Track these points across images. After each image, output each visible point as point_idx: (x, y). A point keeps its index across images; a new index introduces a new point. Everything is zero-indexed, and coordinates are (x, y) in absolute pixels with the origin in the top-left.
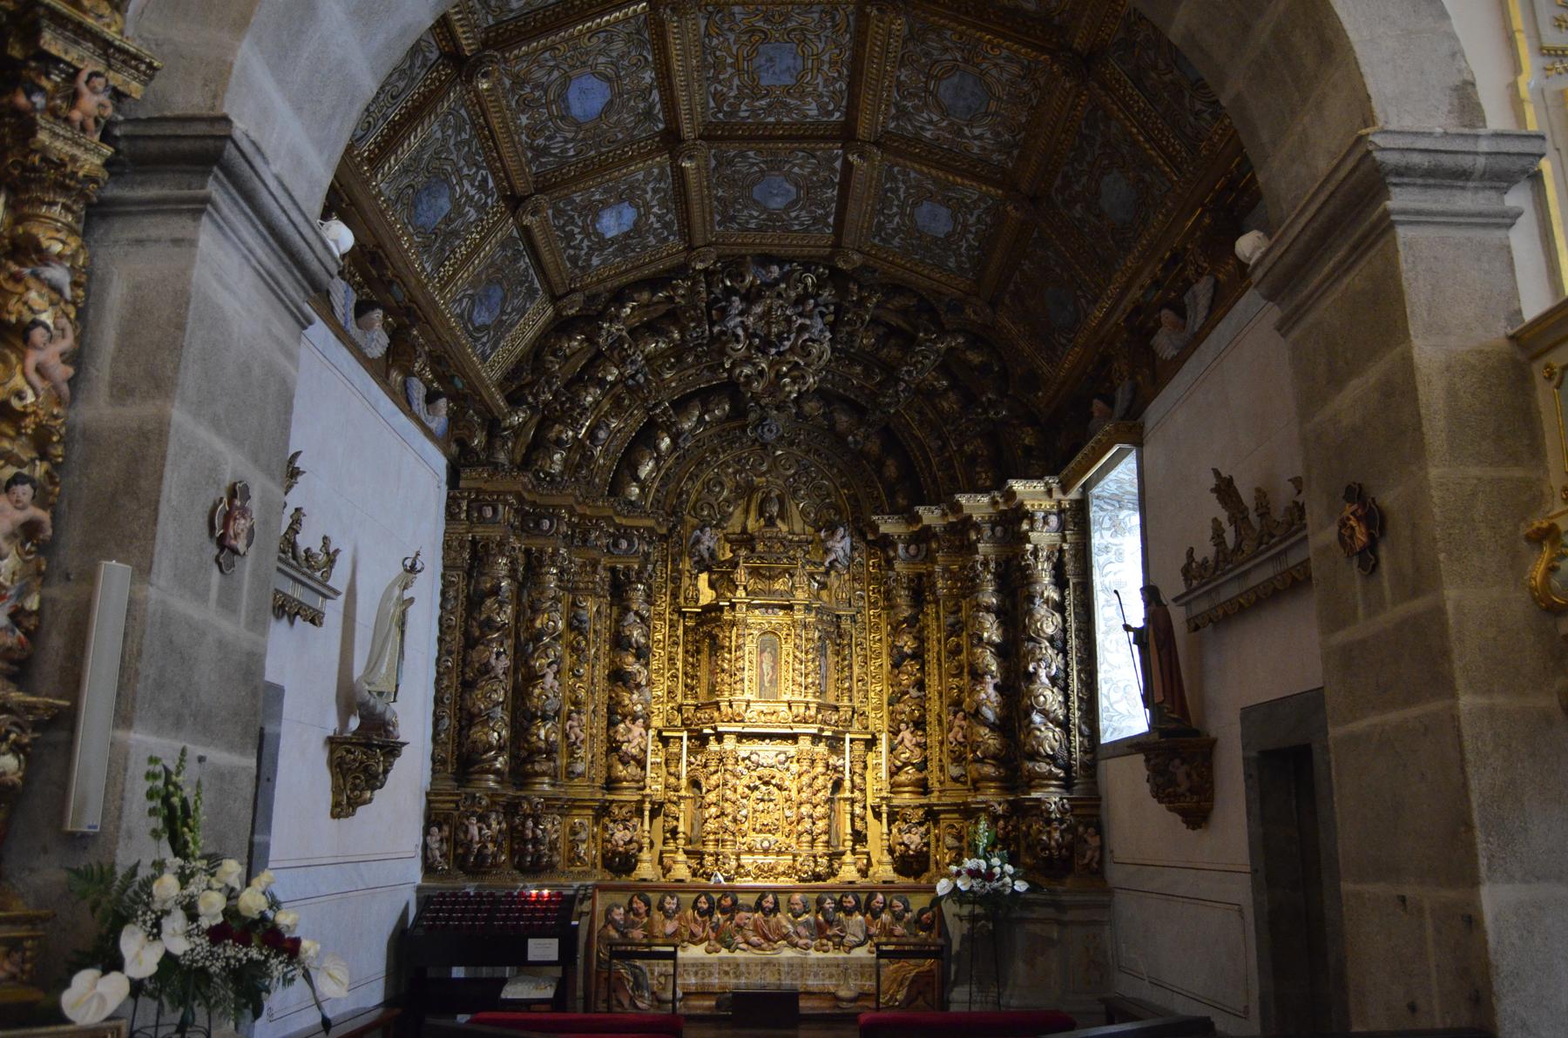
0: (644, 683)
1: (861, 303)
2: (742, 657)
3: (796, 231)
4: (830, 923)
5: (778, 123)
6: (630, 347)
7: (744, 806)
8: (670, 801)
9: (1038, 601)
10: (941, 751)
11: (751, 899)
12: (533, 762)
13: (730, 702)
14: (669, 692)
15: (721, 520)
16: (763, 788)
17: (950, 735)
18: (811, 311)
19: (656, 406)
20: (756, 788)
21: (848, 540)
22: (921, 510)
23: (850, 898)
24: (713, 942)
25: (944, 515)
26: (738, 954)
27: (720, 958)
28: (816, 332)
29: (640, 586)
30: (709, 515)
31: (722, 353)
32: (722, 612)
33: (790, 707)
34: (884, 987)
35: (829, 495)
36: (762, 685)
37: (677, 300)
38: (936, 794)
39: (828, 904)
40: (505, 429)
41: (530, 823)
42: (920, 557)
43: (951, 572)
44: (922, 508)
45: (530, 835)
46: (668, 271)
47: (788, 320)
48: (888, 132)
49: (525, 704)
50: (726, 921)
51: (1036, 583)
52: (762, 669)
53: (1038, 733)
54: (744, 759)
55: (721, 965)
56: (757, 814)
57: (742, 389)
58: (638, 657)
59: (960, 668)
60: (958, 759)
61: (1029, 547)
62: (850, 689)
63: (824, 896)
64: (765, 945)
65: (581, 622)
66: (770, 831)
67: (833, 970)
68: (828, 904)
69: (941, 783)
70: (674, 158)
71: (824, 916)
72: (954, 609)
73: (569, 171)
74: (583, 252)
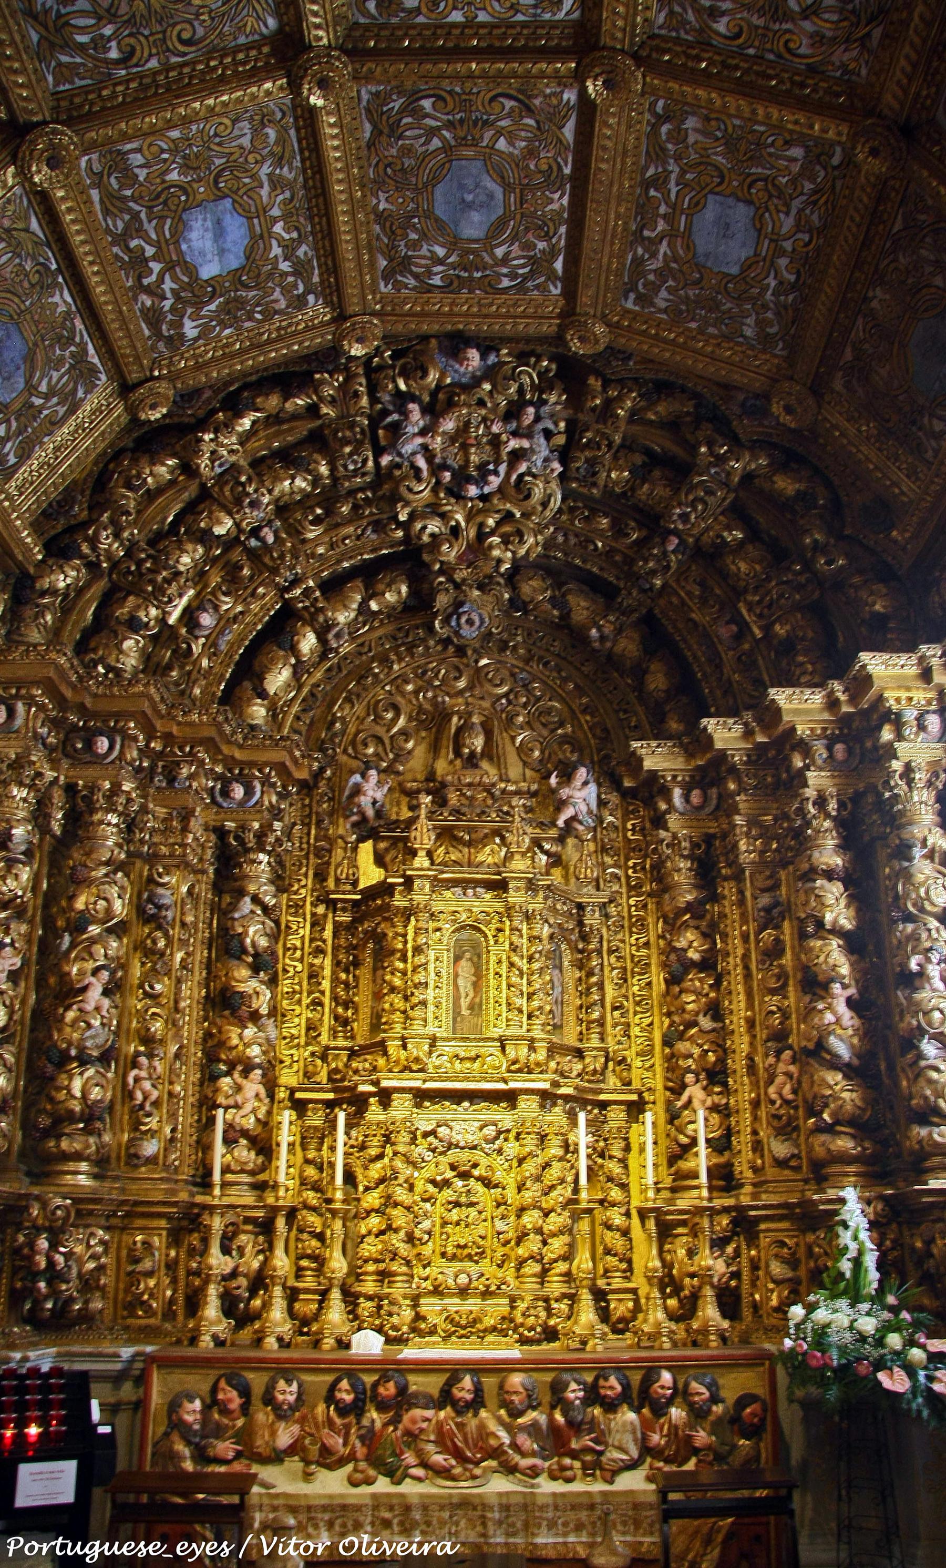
0: (264, 1011)
1: (606, 412)
2: (425, 966)
3: (505, 290)
4: (575, 1427)
5: (470, 23)
6: (250, 480)
7: (426, 1215)
8: (306, 1206)
9: (917, 852)
10: (755, 1118)
11: (432, 1384)
12: (58, 1137)
13: (403, 1038)
14: (308, 1029)
15: (395, 760)
16: (459, 1183)
17: (772, 1090)
18: (530, 426)
19: (295, 582)
20: (447, 1183)
21: (592, 788)
22: (710, 724)
23: (613, 1381)
24: (362, 1465)
25: (748, 734)
26: (408, 1488)
27: (374, 1496)
28: (538, 459)
29: (263, 857)
30: (376, 754)
31: (395, 498)
32: (392, 895)
33: (503, 1048)
34: (676, 1549)
35: (561, 724)
36: (457, 1013)
37: (325, 410)
38: (748, 1189)
39: (574, 1393)
40: (43, 594)
41: (43, 1243)
42: (708, 810)
43: (760, 825)
44: (713, 721)
45: (43, 1264)
46: (306, 358)
47: (496, 442)
48: (652, 37)
49: (51, 1036)
50: (386, 1425)
51: (911, 823)
52: (456, 986)
53: (934, 1075)
54: (426, 1135)
55: (376, 1508)
56: (449, 1229)
57: (426, 557)
58: (256, 969)
59: (782, 976)
60: (786, 1129)
61: (897, 765)
62: (601, 1022)
63: (566, 1376)
64: (458, 1471)
65: (159, 907)
66: (470, 1257)
67: (583, 1515)
68: (574, 1393)
69: (755, 1170)
70: (294, 87)
71: (565, 1414)
72: (769, 883)
73: (114, 95)
74: (167, 304)
